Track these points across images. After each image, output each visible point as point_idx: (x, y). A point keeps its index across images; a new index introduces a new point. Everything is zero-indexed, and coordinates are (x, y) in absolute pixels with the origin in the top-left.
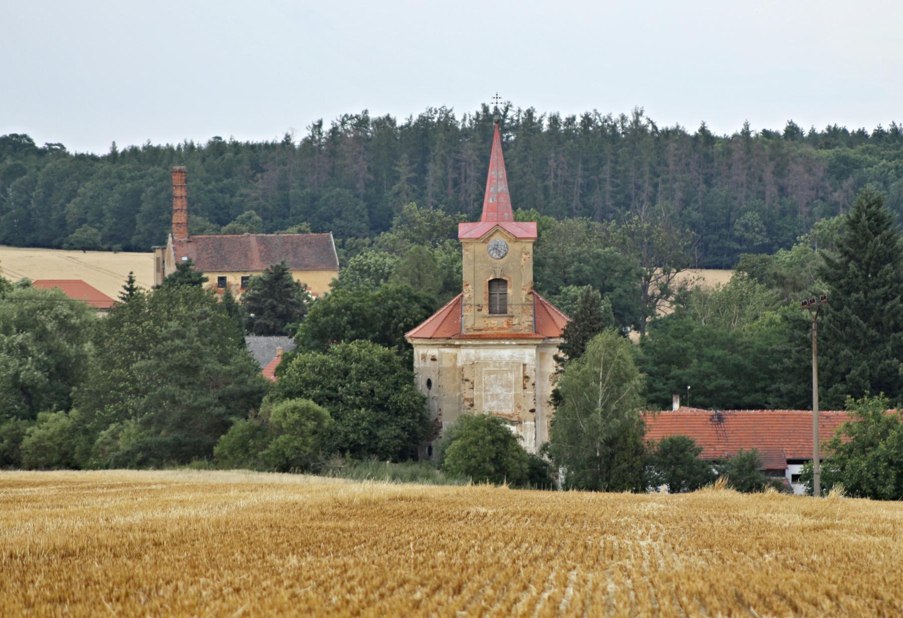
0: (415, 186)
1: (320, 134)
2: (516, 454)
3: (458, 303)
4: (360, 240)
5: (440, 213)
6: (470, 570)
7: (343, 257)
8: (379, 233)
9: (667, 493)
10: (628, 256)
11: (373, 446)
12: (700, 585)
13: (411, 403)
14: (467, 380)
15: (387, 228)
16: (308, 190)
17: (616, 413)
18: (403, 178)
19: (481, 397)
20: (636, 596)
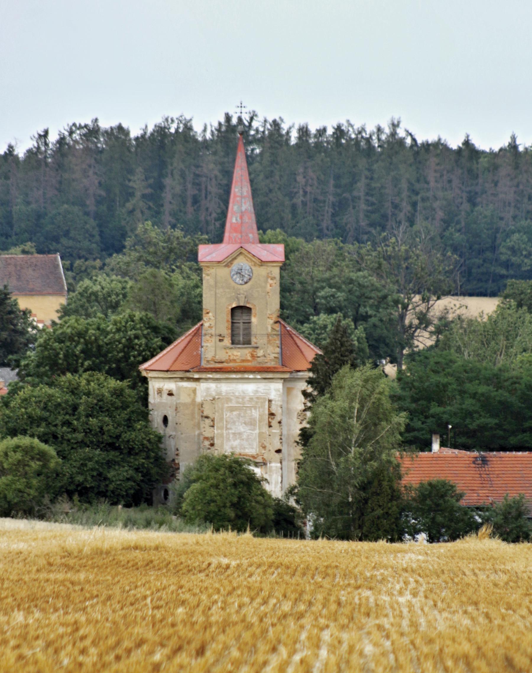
0: (151, 204)
1: (46, 144)
2: (260, 498)
3: (198, 333)
4: (90, 263)
5: (178, 233)
6: (214, 630)
7: (71, 281)
8: (110, 255)
9: (425, 542)
10: (383, 282)
11: (102, 489)
12: (466, 647)
13: (145, 442)
14: (207, 417)
15: (120, 249)
16: (34, 206)
17: (373, 457)
18: (138, 194)
19: (222, 435)
20: (396, 660)
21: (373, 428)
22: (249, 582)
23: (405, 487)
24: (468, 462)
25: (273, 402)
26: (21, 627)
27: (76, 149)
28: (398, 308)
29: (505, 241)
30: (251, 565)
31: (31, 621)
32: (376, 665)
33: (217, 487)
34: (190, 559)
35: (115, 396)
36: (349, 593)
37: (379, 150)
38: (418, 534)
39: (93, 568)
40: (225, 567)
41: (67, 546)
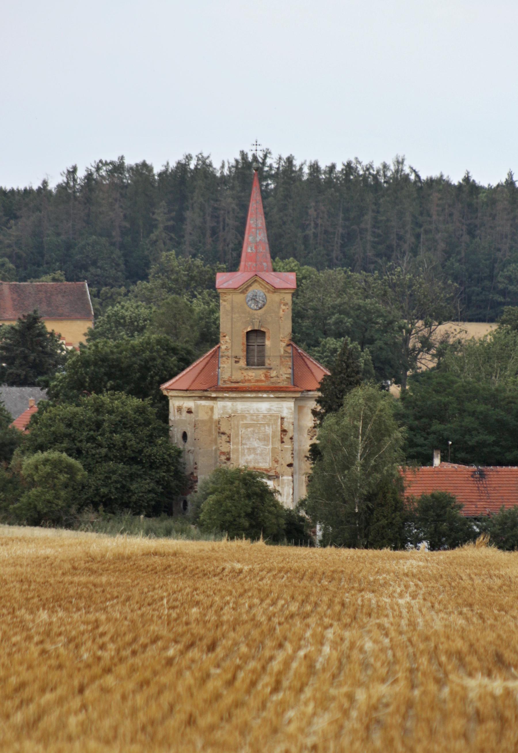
0: (173, 235)
1: (75, 180)
2: (273, 509)
3: (215, 355)
5: (198, 262)
6: (224, 628)
7: (98, 306)
8: (135, 283)
9: (427, 551)
11: (125, 499)
12: (459, 644)
13: (166, 456)
14: (223, 433)
15: (145, 277)
16: (63, 237)
17: (376, 469)
18: (161, 226)
19: (237, 450)
20: (394, 656)
21: (376, 443)
22: (259, 585)
23: (408, 498)
24: (467, 476)
25: (285, 420)
26: (45, 624)
27: (104, 184)
28: (402, 332)
29: (502, 271)
30: (262, 570)
31: (54, 619)
32: (375, 660)
33: (231, 498)
34: (206, 565)
35: (138, 414)
36: (352, 595)
37: (385, 185)
38: (420, 543)
39: (115, 572)
40: (238, 571)
41: (91, 552)
